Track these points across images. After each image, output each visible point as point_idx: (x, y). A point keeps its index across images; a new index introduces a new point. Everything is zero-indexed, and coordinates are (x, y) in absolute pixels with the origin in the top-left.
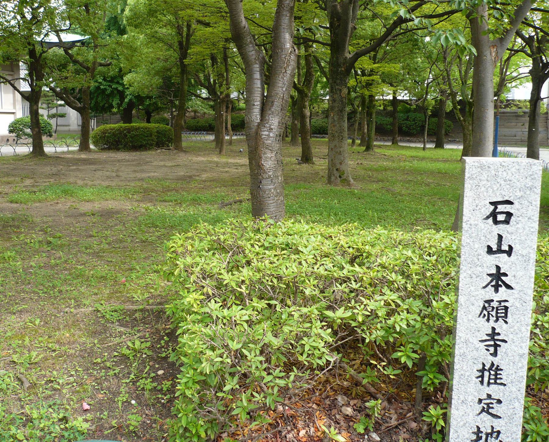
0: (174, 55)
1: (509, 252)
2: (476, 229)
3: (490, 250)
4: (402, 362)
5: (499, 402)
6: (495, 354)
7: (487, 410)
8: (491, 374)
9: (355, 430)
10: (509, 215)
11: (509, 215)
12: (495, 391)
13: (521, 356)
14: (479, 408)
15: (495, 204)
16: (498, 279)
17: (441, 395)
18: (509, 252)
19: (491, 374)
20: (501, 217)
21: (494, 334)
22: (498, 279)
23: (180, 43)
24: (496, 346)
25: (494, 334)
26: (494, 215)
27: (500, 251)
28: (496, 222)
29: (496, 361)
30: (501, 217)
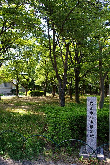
0: (44, 77)
1: (93, 109)
2: (89, 106)
3: (90, 109)
4: (107, 159)
5: (93, 131)
6: (92, 124)
7: (91, 132)
8: (92, 127)
9: (7, 122)
10: (93, 104)
11: (93, 104)
12: (92, 129)
13: (96, 124)
14: (90, 132)
15: (91, 103)
16: (92, 113)
17: (85, 129)
18: (93, 109)
19: (92, 127)
20: (91, 105)
21: (92, 121)
22: (92, 113)
23: (46, 75)
24: (92, 123)
25: (92, 121)
26: (91, 104)
27: (92, 109)
28: (91, 105)
29: (91, 106)
30: (91, 105)
